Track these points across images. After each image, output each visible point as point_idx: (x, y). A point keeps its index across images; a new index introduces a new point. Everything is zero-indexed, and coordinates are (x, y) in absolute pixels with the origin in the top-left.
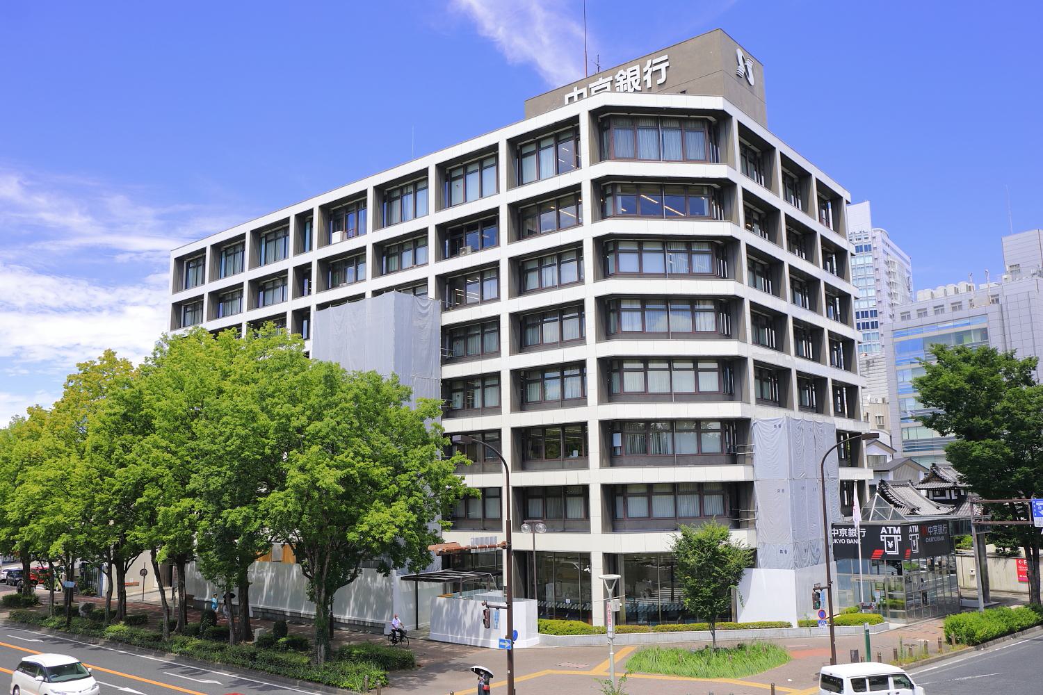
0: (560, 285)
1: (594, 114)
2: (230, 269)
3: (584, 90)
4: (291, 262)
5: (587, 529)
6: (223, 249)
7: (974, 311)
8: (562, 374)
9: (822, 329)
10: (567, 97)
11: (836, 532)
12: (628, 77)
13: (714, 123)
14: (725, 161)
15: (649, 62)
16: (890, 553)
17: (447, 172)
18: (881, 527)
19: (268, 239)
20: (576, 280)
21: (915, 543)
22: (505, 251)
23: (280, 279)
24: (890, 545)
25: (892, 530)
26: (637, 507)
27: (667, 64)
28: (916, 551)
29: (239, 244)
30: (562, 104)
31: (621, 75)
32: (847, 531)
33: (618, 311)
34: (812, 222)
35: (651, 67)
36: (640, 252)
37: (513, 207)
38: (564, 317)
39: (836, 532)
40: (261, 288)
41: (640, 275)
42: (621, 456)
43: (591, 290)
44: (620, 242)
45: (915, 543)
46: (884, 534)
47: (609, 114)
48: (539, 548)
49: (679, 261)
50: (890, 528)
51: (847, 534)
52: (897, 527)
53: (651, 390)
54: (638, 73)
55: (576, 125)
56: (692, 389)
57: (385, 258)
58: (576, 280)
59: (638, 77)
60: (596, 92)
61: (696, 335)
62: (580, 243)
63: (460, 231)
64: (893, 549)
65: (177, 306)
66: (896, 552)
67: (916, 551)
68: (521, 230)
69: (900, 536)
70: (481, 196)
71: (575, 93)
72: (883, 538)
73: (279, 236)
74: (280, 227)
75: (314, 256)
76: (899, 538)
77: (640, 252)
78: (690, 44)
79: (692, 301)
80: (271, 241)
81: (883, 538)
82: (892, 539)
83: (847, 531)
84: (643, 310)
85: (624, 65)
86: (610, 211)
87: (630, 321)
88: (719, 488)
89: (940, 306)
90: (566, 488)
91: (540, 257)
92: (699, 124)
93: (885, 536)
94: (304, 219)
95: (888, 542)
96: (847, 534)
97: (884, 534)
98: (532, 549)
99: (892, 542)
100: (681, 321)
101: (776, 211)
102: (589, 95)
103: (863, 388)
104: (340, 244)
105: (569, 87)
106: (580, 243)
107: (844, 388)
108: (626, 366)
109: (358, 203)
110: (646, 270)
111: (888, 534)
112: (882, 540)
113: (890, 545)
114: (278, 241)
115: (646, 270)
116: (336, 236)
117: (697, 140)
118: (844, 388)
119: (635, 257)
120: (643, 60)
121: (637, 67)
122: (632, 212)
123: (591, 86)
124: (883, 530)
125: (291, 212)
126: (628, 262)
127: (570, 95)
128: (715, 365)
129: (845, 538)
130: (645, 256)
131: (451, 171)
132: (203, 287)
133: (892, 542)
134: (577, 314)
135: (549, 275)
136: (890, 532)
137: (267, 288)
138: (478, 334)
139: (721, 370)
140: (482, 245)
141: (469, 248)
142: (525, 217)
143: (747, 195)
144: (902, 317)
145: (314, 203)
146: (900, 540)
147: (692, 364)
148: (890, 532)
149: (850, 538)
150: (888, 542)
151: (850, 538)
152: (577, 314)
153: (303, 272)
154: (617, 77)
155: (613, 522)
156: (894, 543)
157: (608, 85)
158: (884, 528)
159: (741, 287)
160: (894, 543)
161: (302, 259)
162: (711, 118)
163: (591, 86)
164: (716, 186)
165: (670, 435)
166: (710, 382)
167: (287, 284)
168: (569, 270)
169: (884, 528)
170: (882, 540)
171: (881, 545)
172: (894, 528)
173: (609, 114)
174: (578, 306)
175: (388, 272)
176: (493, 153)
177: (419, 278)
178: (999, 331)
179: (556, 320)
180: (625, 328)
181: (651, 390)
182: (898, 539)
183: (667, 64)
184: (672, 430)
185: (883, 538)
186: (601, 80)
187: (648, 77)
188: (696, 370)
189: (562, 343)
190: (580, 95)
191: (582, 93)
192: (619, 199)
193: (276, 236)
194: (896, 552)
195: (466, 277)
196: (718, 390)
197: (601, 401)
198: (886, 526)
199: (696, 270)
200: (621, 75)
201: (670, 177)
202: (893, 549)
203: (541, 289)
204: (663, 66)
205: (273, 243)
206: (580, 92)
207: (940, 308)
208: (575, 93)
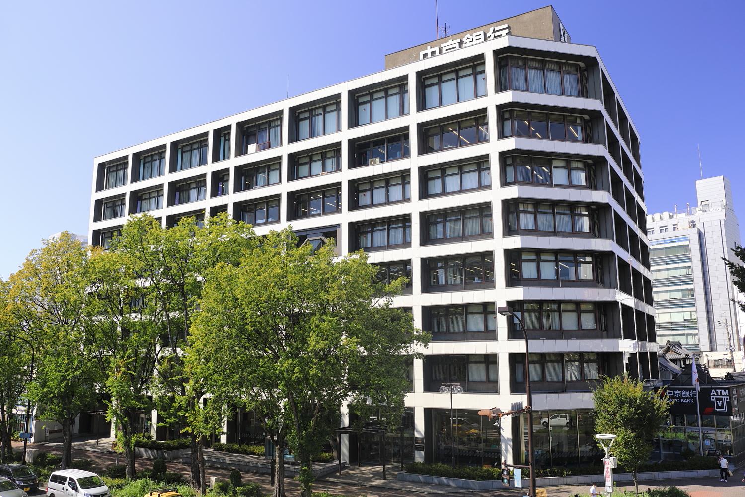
0: (389, 203)
1: (496, 53)
3: (436, 49)
4: (210, 168)
5: (496, 391)
6: (142, 157)
7: (678, 233)
10: (421, 53)
11: (671, 393)
12: (474, 40)
14: (598, 142)
15: (492, 30)
16: (719, 410)
17: (297, 114)
18: (711, 390)
19: (184, 150)
20: (402, 199)
22: (414, 162)
23: (195, 182)
24: (720, 404)
25: (721, 392)
27: (507, 31)
29: (121, 164)
30: (417, 59)
31: (468, 38)
32: (682, 392)
33: (518, 212)
35: (493, 33)
37: (421, 126)
38: (391, 226)
39: (671, 393)
40: (179, 191)
42: (520, 331)
43: (415, 207)
44: (390, 180)
46: (714, 395)
47: (507, 54)
48: (456, 406)
50: (719, 390)
51: (681, 395)
52: (725, 390)
53: (543, 277)
55: (338, 100)
57: (295, 167)
58: (402, 199)
60: (446, 50)
62: (339, 184)
63: (367, 145)
64: (722, 407)
65: (99, 203)
66: (726, 411)
69: (728, 397)
70: (387, 118)
71: (429, 51)
72: (713, 398)
73: (155, 158)
74: (157, 152)
75: (232, 163)
76: (727, 398)
78: (527, 17)
80: (113, 172)
81: (713, 398)
82: (722, 399)
83: (682, 392)
85: (471, 30)
87: (526, 221)
89: (665, 226)
90: (468, 356)
91: (372, 181)
92: (573, 69)
93: (715, 397)
94: (222, 134)
95: (718, 401)
96: (681, 395)
97: (714, 395)
98: (450, 407)
99: (721, 401)
102: (440, 52)
104: (254, 154)
105: (423, 45)
106: (339, 184)
108: (524, 257)
109: (201, 142)
111: (718, 395)
112: (712, 400)
113: (720, 404)
114: (119, 172)
116: (252, 148)
120: (485, 28)
121: (482, 33)
123: (442, 45)
124: (713, 392)
125: (210, 128)
127: (425, 52)
129: (679, 398)
131: (299, 113)
132: (339, 133)
133: (721, 401)
134: (442, 219)
135: (379, 195)
136: (719, 394)
137: (143, 198)
138: (385, 229)
139: (594, 263)
144: (661, 230)
145: (232, 121)
146: (728, 400)
147: (591, 258)
148: (719, 394)
149: (684, 398)
150: (718, 401)
151: (684, 398)
152: (478, 214)
153: (220, 178)
154: (464, 40)
156: (722, 403)
157: (457, 46)
158: (713, 390)
160: (722, 403)
161: (220, 166)
162: (582, 64)
163: (442, 45)
167: (124, 204)
168: (396, 192)
169: (713, 390)
170: (712, 400)
172: (723, 390)
173: (507, 54)
174: (405, 219)
175: (298, 178)
176: (278, 117)
177: (378, 174)
179: (385, 229)
180: (523, 226)
181: (543, 277)
183: (507, 31)
184: (559, 310)
186: (451, 42)
189: (389, 246)
190: (433, 53)
191: (435, 51)
193: (191, 147)
195: (310, 195)
196: (592, 279)
198: (715, 389)
200: (468, 38)
201: (558, 107)
202: (722, 407)
203: (444, 193)
205: (150, 164)
206: (433, 50)
207: (664, 228)
208: (429, 51)
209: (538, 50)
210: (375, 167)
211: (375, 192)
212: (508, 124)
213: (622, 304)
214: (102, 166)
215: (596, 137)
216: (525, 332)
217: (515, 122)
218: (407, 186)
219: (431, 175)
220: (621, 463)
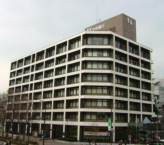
2: (40, 68)
8: (76, 89)
9: (138, 46)
13: (110, 37)
41: (92, 69)
49: (100, 66)
61: (103, 81)
79: (102, 87)
84: (92, 76)
94: (34, 55)
100: (100, 78)
103: (152, 73)
110: (93, 80)
115: (93, 80)
117: (106, 40)
119: (91, 77)
126: (89, 78)
128: (107, 88)
130: (93, 64)
155: (82, 120)
159: (114, 72)
166: (105, 104)
188: (103, 76)
197: (81, 121)
199: (104, 80)
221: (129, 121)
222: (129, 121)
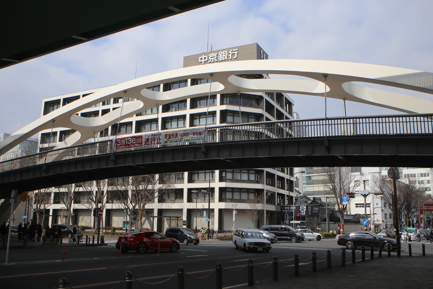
10: (200, 58)
15: (231, 50)
18: (300, 206)
21: (310, 212)
26: (229, 195)
27: (237, 52)
28: (310, 214)
34: (283, 111)
36: (233, 116)
45: (310, 212)
54: (227, 53)
56: (246, 198)
59: (227, 55)
66: (304, 214)
67: (310, 214)
68: (193, 106)
77: (233, 116)
86: (225, 102)
88: (253, 191)
101: (273, 107)
107: (234, 220)
118: (234, 220)
121: (227, 51)
122: (231, 103)
123: (209, 55)
124: (301, 207)
127: (201, 57)
140: (178, 109)
141: (174, 109)
142: (195, 101)
143: (267, 101)
154: (219, 54)
157: (216, 56)
163: (209, 55)
164: (257, 97)
165: (239, 174)
171: (300, 212)
178: (338, 176)
182: (305, 210)
183: (237, 52)
185: (300, 210)
186: (213, 54)
187: (230, 55)
192: (228, 99)
194: (304, 214)
204: (236, 52)
206: (205, 57)
208: (203, 57)
209: (149, 99)
210: (173, 112)
211: (201, 119)
212: (225, 99)
213: (277, 176)
214: (46, 103)
215: (260, 105)
216: (338, 202)
217: (228, 99)
218: (215, 118)
219: (195, 117)
220: (294, 240)
221: (276, 204)
222: (276, 204)
